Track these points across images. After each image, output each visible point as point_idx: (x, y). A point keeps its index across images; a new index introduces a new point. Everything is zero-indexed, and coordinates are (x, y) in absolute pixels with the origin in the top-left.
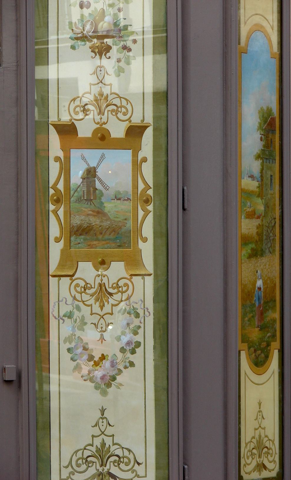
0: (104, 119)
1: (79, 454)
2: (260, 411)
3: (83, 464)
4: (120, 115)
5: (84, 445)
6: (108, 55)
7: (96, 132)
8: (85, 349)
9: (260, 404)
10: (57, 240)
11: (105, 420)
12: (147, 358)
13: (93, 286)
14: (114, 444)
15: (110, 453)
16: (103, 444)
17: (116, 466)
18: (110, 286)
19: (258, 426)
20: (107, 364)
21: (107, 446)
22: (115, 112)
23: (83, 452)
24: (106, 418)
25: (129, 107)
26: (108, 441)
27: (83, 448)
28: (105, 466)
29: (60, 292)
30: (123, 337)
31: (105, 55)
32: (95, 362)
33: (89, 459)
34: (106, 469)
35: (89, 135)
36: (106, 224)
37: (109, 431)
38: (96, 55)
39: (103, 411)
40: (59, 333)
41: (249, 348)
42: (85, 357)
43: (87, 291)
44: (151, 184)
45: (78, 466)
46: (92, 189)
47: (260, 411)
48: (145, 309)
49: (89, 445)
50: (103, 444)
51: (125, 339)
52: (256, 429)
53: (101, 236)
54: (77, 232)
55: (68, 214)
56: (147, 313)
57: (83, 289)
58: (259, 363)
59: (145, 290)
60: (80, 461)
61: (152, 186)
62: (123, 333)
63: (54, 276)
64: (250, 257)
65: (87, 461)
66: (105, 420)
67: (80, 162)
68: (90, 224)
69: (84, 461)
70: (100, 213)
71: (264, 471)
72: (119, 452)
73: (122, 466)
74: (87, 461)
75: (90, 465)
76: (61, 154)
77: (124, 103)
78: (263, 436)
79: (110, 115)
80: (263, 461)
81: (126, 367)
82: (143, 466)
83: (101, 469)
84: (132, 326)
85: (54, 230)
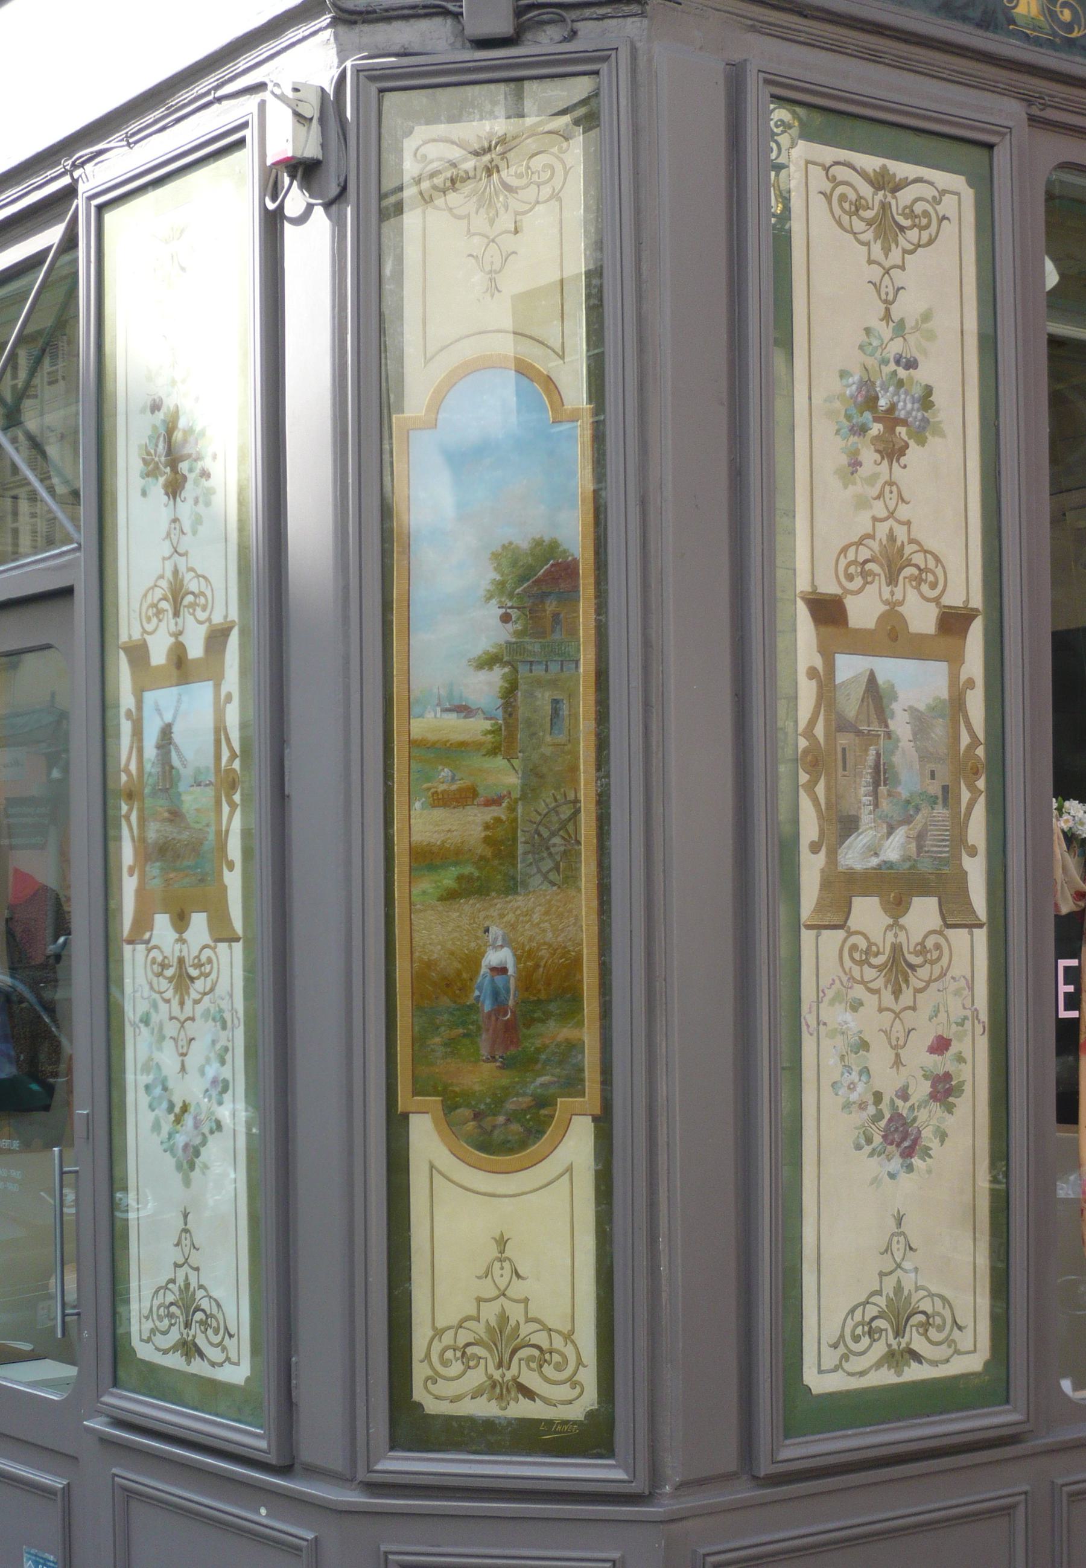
0: (899, 596)
1: (447, 1339)
2: (186, 1231)
3: (457, 1360)
4: (925, 588)
5: (460, 1317)
6: (903, 460)
7: (883, 618)
8: (165, 1089)
9: (186, 1216)
10: (815, 848)
11: (506, 1265)
12: (234, 1112)
13: (870, 205)
14: (528, 1320)
15: (519, 1340)
16: (503, 1318)
17: (533, 1370)
18: (911, 950)
19: (183, 1260)
20: (189, 1120)
21: (512, 1322)
22: (918, 580)
23: (456, 1334)
24: (509, 1259)
25: (939, 571)
26: (516, 1313)
27: (455, 1323)
28: (509, 1369)
29: (135, 964)
30: (207, 1069)
31: (898, 461)
32: (176, 1115)
33: (470, 1350)
34: (509, 1375)
35: (871, 624)
36: (185, 835)
37: (518, 1289)
38: (883, 458)
39: (502, 1243)
40: (137, 1047)
41: (450, 1108)
42: (165, 1105)
43: (861, 212)
44: (981, 736)
45: (445, 1363)
46: (167, 768)
47: (186, 1231)
48: (233, 1010)
49: (468, 1318)
50: (503, 1318)
51: (211, 1071)
52: (177, 1266)
53: (184, 873)
54: (148, 853)
55: (142, 820)
56: (236, 1021)
57: (853, 208)
58: (505, 1133)
59: (230, 966)
60: (449, 1354)
61: (982, 741)
62: (208, 1060)
63: (809, 927)
64: (450, 896)
65: (464, 1354)
66: (506, 1265)
67: (163, 703)
68: (166, 837)
69: (459, 1354)
70: (175, 815)
71: (198, 1359)
72: (541, 1339)
73: (548, 1370)
74: (464, 1354)
75: (472, 1363)
76: (818, 663)
77: (931, 563)
78: (194, 1284)
79: (908, 586)
80: (194, 1337)
81: (212, 1132)
82: (235, 1339)
83: (497, 1375)
84: (218, 1047)
85: (128, 854)
